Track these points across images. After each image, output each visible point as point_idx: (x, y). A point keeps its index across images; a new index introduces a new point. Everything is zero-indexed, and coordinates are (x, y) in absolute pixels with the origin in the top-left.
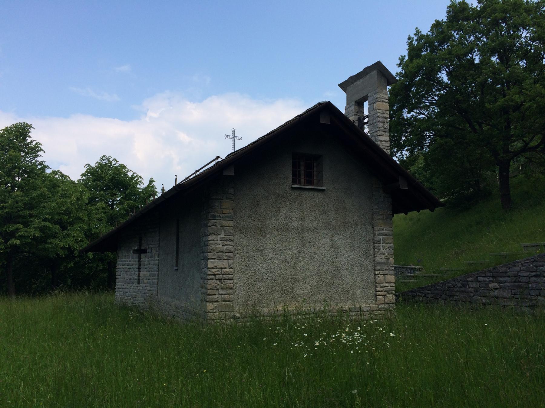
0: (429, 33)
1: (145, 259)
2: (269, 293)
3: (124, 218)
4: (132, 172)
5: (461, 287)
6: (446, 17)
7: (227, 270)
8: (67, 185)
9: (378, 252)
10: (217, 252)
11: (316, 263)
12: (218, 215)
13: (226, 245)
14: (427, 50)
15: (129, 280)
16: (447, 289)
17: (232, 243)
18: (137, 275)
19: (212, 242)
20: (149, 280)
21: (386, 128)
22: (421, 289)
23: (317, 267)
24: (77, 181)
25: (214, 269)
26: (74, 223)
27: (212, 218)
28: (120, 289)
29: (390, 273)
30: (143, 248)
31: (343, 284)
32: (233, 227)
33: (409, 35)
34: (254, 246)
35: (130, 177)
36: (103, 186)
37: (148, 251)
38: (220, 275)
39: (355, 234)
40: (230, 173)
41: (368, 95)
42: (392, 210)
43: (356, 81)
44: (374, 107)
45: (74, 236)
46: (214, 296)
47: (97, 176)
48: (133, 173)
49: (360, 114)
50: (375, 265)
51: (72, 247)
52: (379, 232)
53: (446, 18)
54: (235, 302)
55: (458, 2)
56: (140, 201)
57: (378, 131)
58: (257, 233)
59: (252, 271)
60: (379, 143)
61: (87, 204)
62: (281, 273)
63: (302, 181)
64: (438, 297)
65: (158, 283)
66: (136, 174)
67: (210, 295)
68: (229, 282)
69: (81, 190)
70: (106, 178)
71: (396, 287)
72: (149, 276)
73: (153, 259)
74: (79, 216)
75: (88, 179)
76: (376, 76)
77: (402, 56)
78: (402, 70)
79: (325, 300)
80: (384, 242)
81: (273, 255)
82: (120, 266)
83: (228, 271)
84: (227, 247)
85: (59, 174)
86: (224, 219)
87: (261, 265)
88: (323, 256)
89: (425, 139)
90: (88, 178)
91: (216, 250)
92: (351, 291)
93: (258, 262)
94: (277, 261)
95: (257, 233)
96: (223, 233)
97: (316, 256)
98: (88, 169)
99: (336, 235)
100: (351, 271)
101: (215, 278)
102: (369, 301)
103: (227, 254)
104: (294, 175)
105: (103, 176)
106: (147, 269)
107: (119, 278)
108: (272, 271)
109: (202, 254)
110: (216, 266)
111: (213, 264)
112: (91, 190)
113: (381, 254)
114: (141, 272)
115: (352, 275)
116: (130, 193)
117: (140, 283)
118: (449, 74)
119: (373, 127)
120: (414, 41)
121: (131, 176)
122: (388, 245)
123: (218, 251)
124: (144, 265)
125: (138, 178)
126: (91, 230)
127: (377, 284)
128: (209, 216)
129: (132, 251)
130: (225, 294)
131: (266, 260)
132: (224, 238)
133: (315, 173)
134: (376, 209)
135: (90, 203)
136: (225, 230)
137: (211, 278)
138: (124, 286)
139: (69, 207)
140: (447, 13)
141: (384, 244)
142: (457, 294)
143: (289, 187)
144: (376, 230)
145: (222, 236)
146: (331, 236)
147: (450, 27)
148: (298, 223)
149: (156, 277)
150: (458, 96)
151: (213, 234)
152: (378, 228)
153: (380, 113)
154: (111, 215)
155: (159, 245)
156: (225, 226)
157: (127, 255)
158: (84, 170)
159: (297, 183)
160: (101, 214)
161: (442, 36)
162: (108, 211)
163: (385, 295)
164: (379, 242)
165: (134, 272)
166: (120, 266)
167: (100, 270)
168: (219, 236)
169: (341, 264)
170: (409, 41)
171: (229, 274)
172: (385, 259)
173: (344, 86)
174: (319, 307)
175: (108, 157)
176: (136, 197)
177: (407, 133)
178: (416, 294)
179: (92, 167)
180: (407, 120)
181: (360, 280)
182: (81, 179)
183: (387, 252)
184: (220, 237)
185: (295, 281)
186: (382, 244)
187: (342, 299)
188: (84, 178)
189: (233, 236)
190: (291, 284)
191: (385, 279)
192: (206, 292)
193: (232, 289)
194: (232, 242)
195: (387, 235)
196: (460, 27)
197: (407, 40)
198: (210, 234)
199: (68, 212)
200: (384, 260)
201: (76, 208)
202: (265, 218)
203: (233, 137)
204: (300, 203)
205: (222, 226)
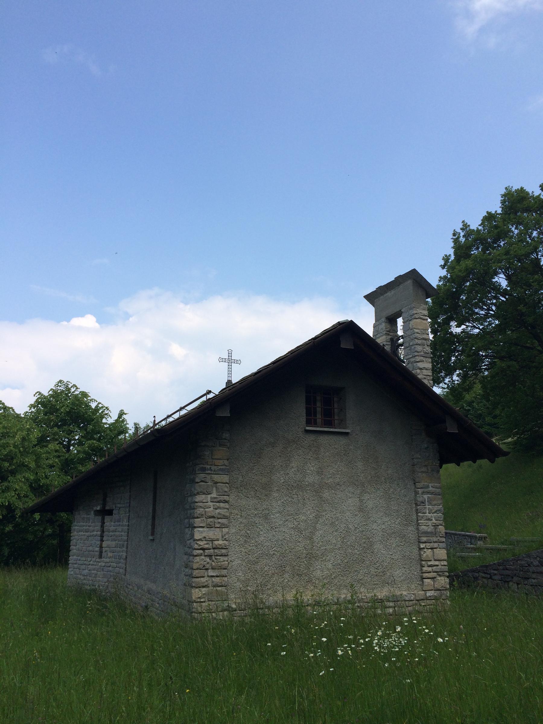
0: (480, 228)
3: (83, 464)
5: (538, 566)
6: (500, 207)
7: (220, 542)
8: (11, 420)
11: (339, 533)
12: (209, 467)
13: (219, 508)
14: (477, 248)
15: (87, 552)
17: (226, 505)
18: (98, 546)
19: (201, 504)
20: (115, 553)
21: (426, 353)
22: (485, 568)
23: (341, 538)
24: (23, 414)
25: (202, 541)
26: (17, 472)
28: (75, 566)
30: (107, 508)
32: (228, 483)
33: (454, 230)
35: (94, 408)
36: (58, 420)
37: (114, 512)
39: (390, 492)
40: (225, 413)
41: (402, 310)
42: (439, 460)
43: (386, 292)
44: (411, 326)
45: (16, 490)
46: (202, 579)
47: (50, 408)
48: (98, 403)
50: (420, 535)
53: (501, 209)
54: (231, 588)
55: (515, 190)
56: (106, 440)
57: (416, 356)
58: (260, 492)
59: (253, 543)
60: (418, 371)
61: (35, 446)
62: (293, 547)
63: (319, 421)
64: (507, 580)
65: (126, 557)
66: (102, 404)
68: (222, 558)
69: (28, 426)
70: (62, 410)
71: (449, 565)
72: (115, 547)
74: (23, 462)
75: (38, 411)
77: (446, 255)
78: (446, 273)
79: (352, 585)
80: (430, 504)
81: (282, 522)
86: (217, 473)
87: (265, 535)
88: (348, 523)
89: (481, 360)
90: (37, 410)
92: (387, 572)
93: (262, 530)
94: (286, 530)
95: (260, 492)
96: (215, 491)
97: (338, 523)
98: (39, 398)
99: (365, 493)
100: (388, 544)
101: (203, 554)
103: (220, 520)
105: (58, 408)
107: (74, 550)
109: (187, 521)
110: (205, 537)
111: (201, 534)
112: (42, 426)
113: (426, 520)
114: (104, 541)
115: (388, 549)
116: (92, 430)
117: (103, 556)
118: (508, 278)
119: (409, 351)
120: (460, 237)
121: (95, 407)
122: (436, 508)
123: (208, 516)
125: (105, 410)
126: (39, 480)
127: (423, 563)
128: (197, 469)
129: (92, 512)
130: (217, 576)
133: (336, 411)
134: (417, 458)
135: (39, 443)
136: (218, 488)
138: (80, 560)
139: (11, 450)
140: (501, 203)
141: (430, 507)
142: (534, 576)
144: (419, 487)
145: (214, 495)
146: (359, 495)
147: (507, 220)
148: (314, 478)
149: (124, 549)
150: (521, 307)
151: (202, 494)
154: (67, 459)
155: (129, 506)
156: (216, 483)
158: (33, 400)
160: (53, 459)
161: (496, 231)
162: (62, 454)
163: (435, 578)
164: (423, 503)
165: (94, 541)
167: (49, 535)
168: (209, 496)
169: (374, 534)
170: (455, 237)
171: (222, 548)
172: (432, 527)
173: (371, 298)
174: (345, 595)
176: (101, 435)
177: (457, 353)
178: (478, 575)
179: (44, 396)
180: (457, 336)
182: (29, 411)
184: (211, 497)
185: (311, 557)
186: (427, 506)
187: (375, 583)
188: (33, 410)
189: (228, 496)
190: (305, 561)
191: (434, 555)
192: (192, 574)
194: (227, 504)
195: (434, 494)
196: (519, 221)
197: (452, 236)
200: (430, 529)
201: (20, 451)
203: (229, 360)
204: (316, 451)
205: (214, 482)
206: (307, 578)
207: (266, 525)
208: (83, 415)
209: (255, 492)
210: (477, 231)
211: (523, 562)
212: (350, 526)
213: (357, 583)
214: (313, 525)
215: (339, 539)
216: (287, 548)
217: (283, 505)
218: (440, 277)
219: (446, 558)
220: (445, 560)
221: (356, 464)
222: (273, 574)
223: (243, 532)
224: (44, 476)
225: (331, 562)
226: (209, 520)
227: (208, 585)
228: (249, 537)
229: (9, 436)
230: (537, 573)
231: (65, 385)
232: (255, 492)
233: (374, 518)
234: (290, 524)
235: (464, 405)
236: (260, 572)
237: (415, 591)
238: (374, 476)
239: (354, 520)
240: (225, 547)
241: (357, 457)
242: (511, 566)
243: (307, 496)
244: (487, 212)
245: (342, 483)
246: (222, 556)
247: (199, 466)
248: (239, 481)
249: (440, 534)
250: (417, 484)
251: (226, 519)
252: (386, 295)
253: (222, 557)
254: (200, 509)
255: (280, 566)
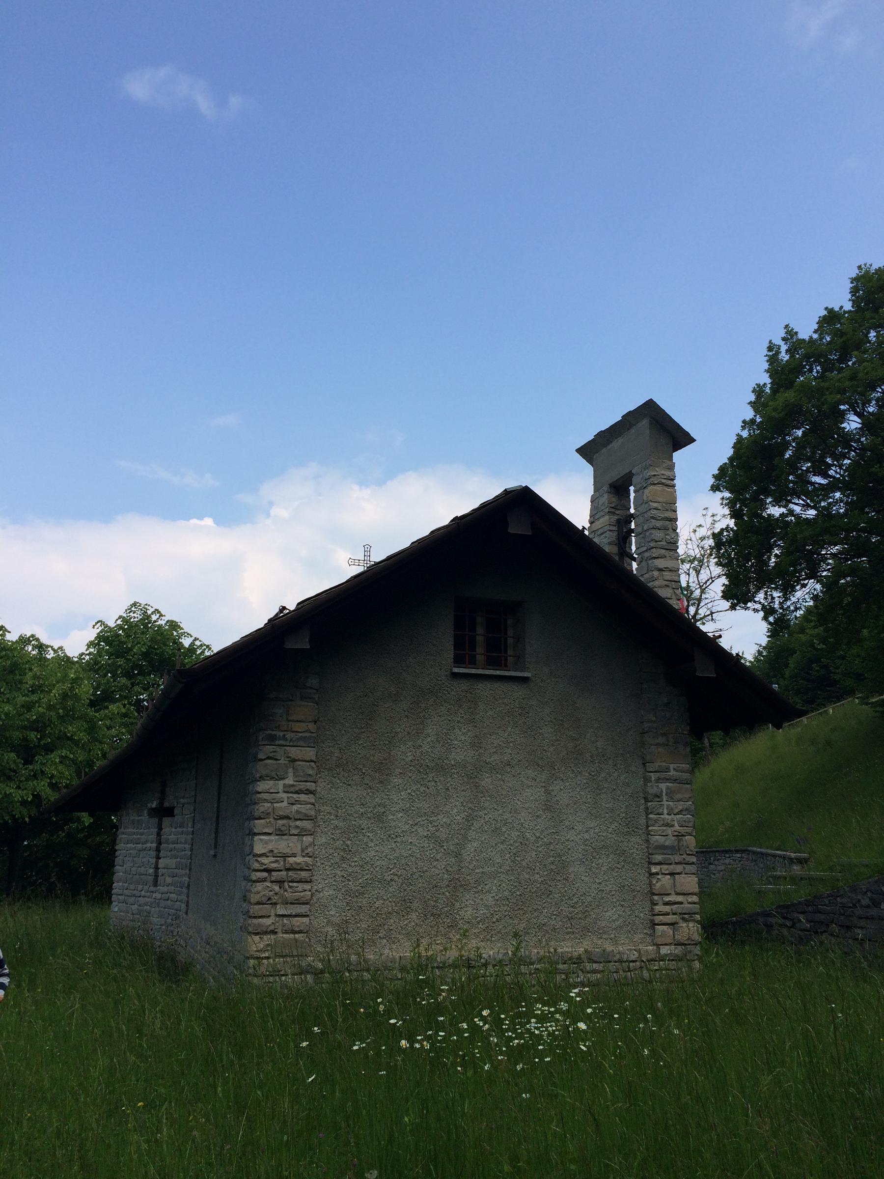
0: (815, 336)
1: (170, 831)
2: (395, 914)
4: (191, 636)
5: (868, 906)
6: (850, 300)
7: (299, 859)
9: (656, 821)
10: (275, 819)
12: (281, 734)
13: (297, 802)
15: (137, 876)
16: (840, 912)
17: (311, 798)
19: (265, 796)
20: (175, 878)
21: (671, 543)
22: (786, 910)
25: (268, 856)
27: (266, 743)
29: (687, 871)
30: (166, 805)
31: (574, 895)
32: (313, 761)
33: (771, 341)
34: (362, 804)
35: (187, 647)
37: (176, 811)
38: (281, 871)
39: (600, 778)
43: (609, 442)
48: (193, 638)
49: (622, 512)
51: (46, 800)
52: (659, 774)
53: (850, 303)
55: (876, 270)
57: (653, 548)
59: (356, 862)
63: (480, 658)
65: (189, 885)
66: (200, 641)
67: (255, 917)
68: (301, 886)
70: (135, 650)
73: (184, 829)
75: (99, 653)
76: (648, 432)
77: (758, 385)
80: (670, 798)
81: (407, 826)
82: (122, 845)
83: (298, 861)
84: (299, 806)
85: (33, 642)
86: (295, 744)
88: (524, 829)
91: (274, 813)
93: (372, 840)
99: (556, 780)
102: (637, 937)
103: (298, 823)
104: (458, 644)
106: (172, 852)
107: (120, 871)
108: (403, 862)
111: (265, 846)
113: (663, 825)
114: (160, 859)
115: (594, 873)
117: (159, 883)
120: (781, 352)
122: (681, 806)
123: (278, 816)
124: (167, 842)
125: (205, 649)
127: (656, 898)
128: (261, 738)
129: (146, 812)
131: (389, 836)
132: (293, 786)
133: (510, 641)
134: (651, 721)
137: (259, 878)
140: (850, 293)
141: (670, 803)
142: (862, 923)
143: (446, 671)
144: (651, 770)
145: (290, 781)
151: (268, 778)
152: (656, 765)
153: (656, 509)
155: (195, 801)
156: (294, 761)
157: (138, 821)
159: (465, 663)
164: (658, 797)
166: (122, 845)
168: (281, 783)
169: (569, 849)
170: (771, 354)
173: (587, 451)
175: (142, 606)
179: (110, 627)
181: (614, 886)
182: (86, 653)
183: (678, 821)
184: (284, 784)
185: (457, 885)
187: (570, 930)
189: (315, 782)
190: (447, 893)
192: (248, 911)
193: (307, 904)
194: (312, 795)
195: (678, 781)
197: (766, 352)
198: (261, 777)
199: (38, 726)
200: (670, 841)
202: (390, 742)
204: (470, 708)
206: (448, 921)
207: (379, 832)
208: (169, 658)
209: (363, 776)
210: (809, 342)
211: (845, 900)
212: (527, 834)
213: (537, 930)
214: (463, 831)
215: (508, 855)
216: (415, 870)
217: (409, 799)
218: (744, 422)
219: (697, 890)
220: (695, 894)
221: (541, 731)
222: (389, 913)
223: (339, 843)
224: (100, 755)
225: (492, 895)
226: (280, 822)
227: (276, 930)
228: (351, 851)
229: (42, 691)
230: (867, 918)
231: (141, 610)
232: (363, 776)
233: (569, 821)
234: (422, 830)
235: (815, 641)
236: (368, 910)
237: (640, 945)
238: (573, 750)
239: (535, 825)
240: (307, 868)
241: (542, 719)
242: (825, 907)
243: (452, 783)
244: (826, 309)
245: (514, 763)
246: (302, 882)
247: (265, 732)
248: (335, 759)
249: (687, 849)
250: (648, 764)
251: (309, 821)
252: (611, 446)
253: (300, 884)
254: (265, 804)
255: (403, 899)
